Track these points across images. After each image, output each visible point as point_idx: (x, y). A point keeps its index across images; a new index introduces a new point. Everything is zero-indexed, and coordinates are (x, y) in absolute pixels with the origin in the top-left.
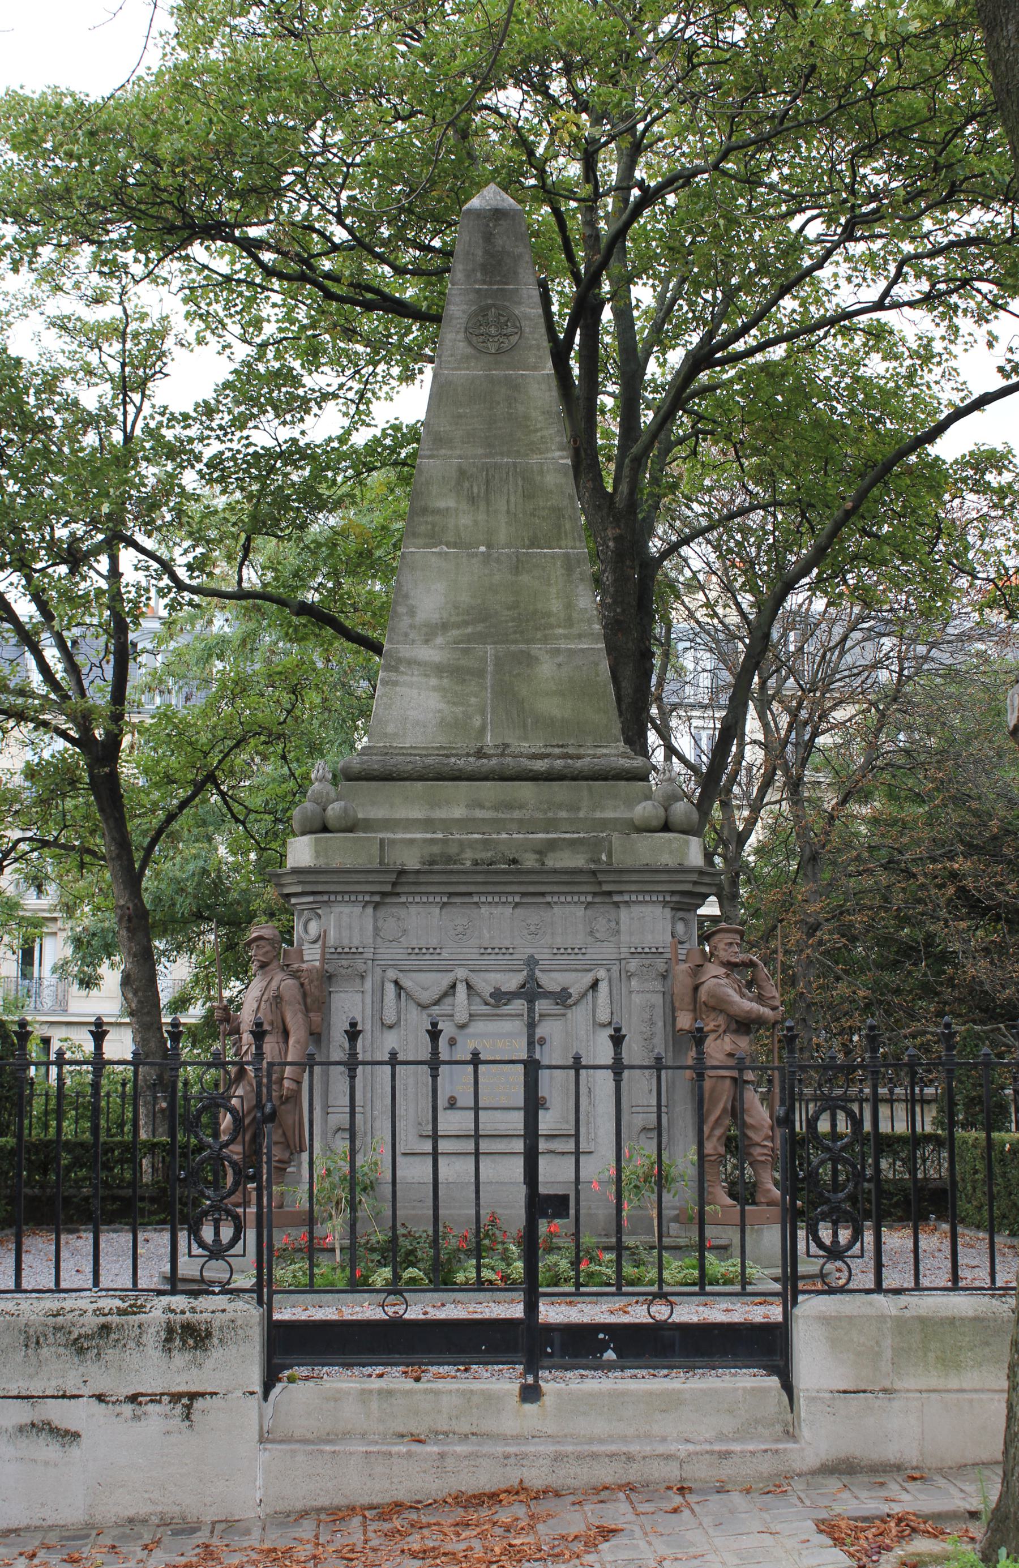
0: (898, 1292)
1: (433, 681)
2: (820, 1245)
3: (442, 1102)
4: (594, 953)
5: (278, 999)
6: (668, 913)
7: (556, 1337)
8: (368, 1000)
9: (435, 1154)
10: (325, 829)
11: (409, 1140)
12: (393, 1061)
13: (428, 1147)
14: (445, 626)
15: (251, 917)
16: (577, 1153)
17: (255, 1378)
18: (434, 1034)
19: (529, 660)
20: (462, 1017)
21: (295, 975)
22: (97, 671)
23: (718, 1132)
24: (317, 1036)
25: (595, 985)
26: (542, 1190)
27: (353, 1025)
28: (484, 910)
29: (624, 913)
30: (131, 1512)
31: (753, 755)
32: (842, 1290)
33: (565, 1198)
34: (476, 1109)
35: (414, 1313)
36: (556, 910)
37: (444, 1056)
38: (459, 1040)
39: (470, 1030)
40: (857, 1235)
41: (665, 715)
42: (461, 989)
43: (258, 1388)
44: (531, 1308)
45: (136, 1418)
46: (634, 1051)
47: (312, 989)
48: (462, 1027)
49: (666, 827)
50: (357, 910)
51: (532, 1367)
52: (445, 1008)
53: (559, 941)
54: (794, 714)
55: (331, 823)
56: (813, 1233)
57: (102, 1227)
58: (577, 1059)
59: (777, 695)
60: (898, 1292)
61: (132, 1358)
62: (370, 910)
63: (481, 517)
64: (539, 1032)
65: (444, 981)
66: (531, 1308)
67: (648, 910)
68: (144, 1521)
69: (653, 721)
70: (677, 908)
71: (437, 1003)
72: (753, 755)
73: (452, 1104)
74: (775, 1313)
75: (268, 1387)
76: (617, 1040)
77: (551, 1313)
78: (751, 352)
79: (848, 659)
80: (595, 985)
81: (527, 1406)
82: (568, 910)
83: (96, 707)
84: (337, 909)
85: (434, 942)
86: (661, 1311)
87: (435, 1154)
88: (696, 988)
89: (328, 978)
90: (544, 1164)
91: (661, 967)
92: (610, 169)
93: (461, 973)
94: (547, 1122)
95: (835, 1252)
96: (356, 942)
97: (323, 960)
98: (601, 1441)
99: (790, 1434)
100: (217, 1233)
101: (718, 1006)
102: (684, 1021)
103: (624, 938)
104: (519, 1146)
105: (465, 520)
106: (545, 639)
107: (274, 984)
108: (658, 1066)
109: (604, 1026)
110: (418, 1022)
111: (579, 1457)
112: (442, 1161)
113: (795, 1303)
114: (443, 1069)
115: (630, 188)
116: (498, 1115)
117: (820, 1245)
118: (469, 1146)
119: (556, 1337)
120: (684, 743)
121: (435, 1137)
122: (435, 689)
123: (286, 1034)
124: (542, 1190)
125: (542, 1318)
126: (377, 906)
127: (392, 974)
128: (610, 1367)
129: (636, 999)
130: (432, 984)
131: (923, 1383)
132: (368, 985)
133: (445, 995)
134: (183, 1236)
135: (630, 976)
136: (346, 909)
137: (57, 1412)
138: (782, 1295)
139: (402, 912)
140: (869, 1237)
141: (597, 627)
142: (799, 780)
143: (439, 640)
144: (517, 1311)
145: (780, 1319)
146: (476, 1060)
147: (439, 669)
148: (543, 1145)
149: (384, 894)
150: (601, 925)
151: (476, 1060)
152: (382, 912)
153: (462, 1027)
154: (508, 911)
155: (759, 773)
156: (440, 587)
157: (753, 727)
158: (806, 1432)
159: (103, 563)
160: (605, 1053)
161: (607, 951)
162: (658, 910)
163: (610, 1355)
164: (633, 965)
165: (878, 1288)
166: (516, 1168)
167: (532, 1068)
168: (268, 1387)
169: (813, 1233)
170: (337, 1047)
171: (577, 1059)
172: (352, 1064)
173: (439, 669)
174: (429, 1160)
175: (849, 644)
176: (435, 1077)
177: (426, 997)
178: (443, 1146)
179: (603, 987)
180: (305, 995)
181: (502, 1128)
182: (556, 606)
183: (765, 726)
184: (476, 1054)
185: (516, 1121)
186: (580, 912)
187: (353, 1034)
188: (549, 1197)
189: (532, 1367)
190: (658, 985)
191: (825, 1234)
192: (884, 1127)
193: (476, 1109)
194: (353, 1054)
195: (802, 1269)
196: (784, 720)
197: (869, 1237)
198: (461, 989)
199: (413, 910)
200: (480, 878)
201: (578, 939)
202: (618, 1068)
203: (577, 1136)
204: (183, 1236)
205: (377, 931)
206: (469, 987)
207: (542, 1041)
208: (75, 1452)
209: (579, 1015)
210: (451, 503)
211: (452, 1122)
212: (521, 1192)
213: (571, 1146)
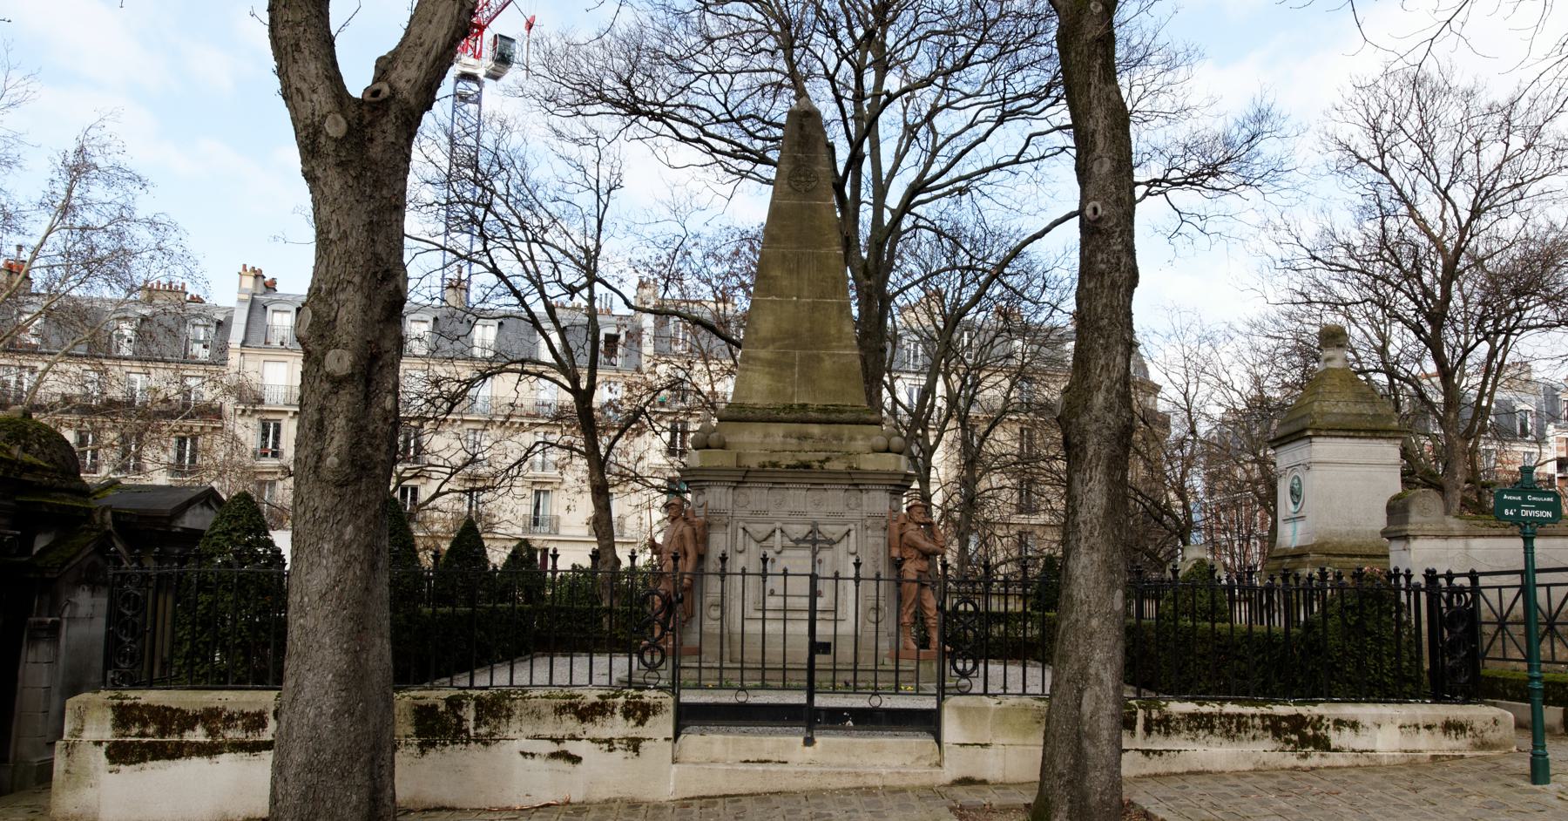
0: (995, 695)
1: (767, 370)
2: (957, 670)
3: (768, 592)
4: (848, 516)
5: (682, 537)
6: (888, 495)
7: (823, 714)
8: (134, 370)
9: (764, 619)
10: (708, 447)
11: (750, 612)
12: (744, 573)
13: (760, 615)
14: (773, 340)
15: (374, 254)
16: (836, 620)
17: (670, 734)
18: (765, 560)
19: (819, 359)
20: (778, 548)
21: (690, 524)
22: (581, 351)
23: (911, 611)
24: (701, 558)
25: (848, 533)
26: (818, 639)
27: (724, 555)
28: (791, 492)
29: (865, 496)
30: (606, 797)
31: (940, 403)
32: (967, 694)
33: (829, 644)
34: (785, 596)
35: (752, 700)
36: (829, 492)
37: (769, 571)
38: (777, 560)
39: (783, 554)
40: (976, 666)
41: (892, 380)
42: (778, 533)
43: (671, 736)
44: (811, 698)
45: (610, 750)
46: (867, 570)
47: (699, 531)
48: (779, 553)
49: (888, 450)
50: (724, 490)
51: (810, 729)
52: (769, 542)
53: (830, 509)
54: (964, 382)
55: (711, 444)
56: (953, 664)
57: (476, 671)
58: (837, 574)
59: (956, 369)
60: (995, 695)
61: (609, 721)
62: (731, 490)
63: (795, 281)
64: (818, 557)
65: (769, 528)
66: (811, 698)
67: (878, 494)
68: (615, 801)
69: (885, 383)
70: (893, 493)
71: (765, 540)
72: (940, 403)
73: (772, 593)
74: (929, 703)
75: (677, 735)
76: (857, 565)
77: (821, 701)
78: (942, 173)
79: (995, 351)
80: (848, 533)
81: (807, 748)
82: (835, 492)
83: (368, 151)
84: (714, 489)
85: (764, 507)
86: (876, 701)
87: (764, 619)
88: (902, 535)
89: (707, 526)
90: (819, 626)
91: (884, 524)
92: (869, 79)
93: (778, 525)
94: (821, 603)
95: (964, 674)
96: (723, 507)
97: (707, 517)
98: (844, 766)
99: (939, 765)
100: (652, 658)
101: (914, 546)
102: (895, 553)
103: (865, 508)
104: (806, 616)
105: (785, 283)
106: (827, 348)
107: (680, 529)
108: (878, 578)
109: (853, 554)
110: (755, 551)
111: (833, 774)
112: (767, 623)
113: (943, 699)
114: (769, 578)
115: (880, 96)
116: (796, 599)
117: (957, 670)
118: (781, 615)
119: (823, 714)
120: (903, 397)
121: (764, 610)
122: (768, 373)
123: (686, 554)
124: (818, 639)
125: (816, 705)
126: (735, 488)
127: (741, 524)
128: (849, 729)
129: (871, 540)
130: (764, 529)
131: (1005, 741)
132: (729, 530)
133: (770, 536)
134: (635, 659)
135: (867, 528)
136: (719, 490)
137: (571, 747)
138: (937, 695)
139: (748, 492)
140: (981, 666)
141: (855, 342)
142: (967, 416)
143: (771, 348)
144: (804, 701)
145: (935, 707)
146: (785, 574)
147: (770, 363)
148: (818, 616)
149: (738, 482)
150: (853, 501)
151: (785, 574)
152: (737, 491)
153: (779, 553)
154: (804, 492)
155: (944, 412)
156: (771, 318)
157: (940, 388)
158: (946, 764)
159: (585, 292)
160: (852, 572)
161: (856, 515)
162: (883, 494)
163: (850, 723)
164: (869, 522)
165: (985, 693)
166: (805, 627)
167: (814, 578)
168: (677, 735)
169: (953, 664)
170: (713, 565)
171: (837, 574)
172: (723, 574)
173: (770, 363)
174: (760, 623)
175: (996, 342)
176: (764, 582)
177: (760, 536)
178: (768, 615)
179: (853, 534)
180: (695, 535)
181: (798, 606)
182: (833, 331)
183: (948, 387)
184: (785, 570)
185: (805, 602)
186: (842, 494)
187: (723, 559)
188: (821, 644)
189: (810, 729)
190: (881, 533)
191: (960, 665)
192: (994, 608)
193: (785, 596)
194: (723, 569)
195: (947, 684)
196: (958, 385)
197: (981, 666)
198: (778, 533)
199: (753, 491)
200: (789, 475)
201: (839, 508)
202: (857, 579)
203: (836, 611)
204: (635, 659)
205: (734, 502)
206: (782, 531)
207: (820, 561)
208: (578, 766)
209: (841, 548)
210: (778, 273)
211: (773, 602)
212: (806, 641)
213: (833, 617)
